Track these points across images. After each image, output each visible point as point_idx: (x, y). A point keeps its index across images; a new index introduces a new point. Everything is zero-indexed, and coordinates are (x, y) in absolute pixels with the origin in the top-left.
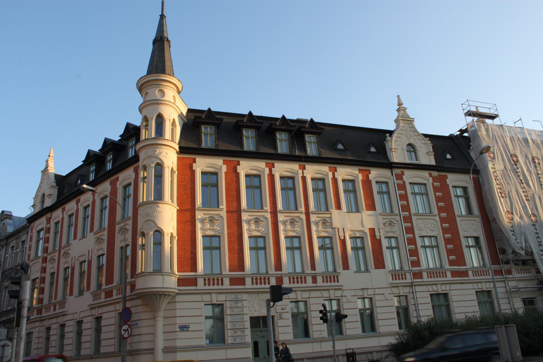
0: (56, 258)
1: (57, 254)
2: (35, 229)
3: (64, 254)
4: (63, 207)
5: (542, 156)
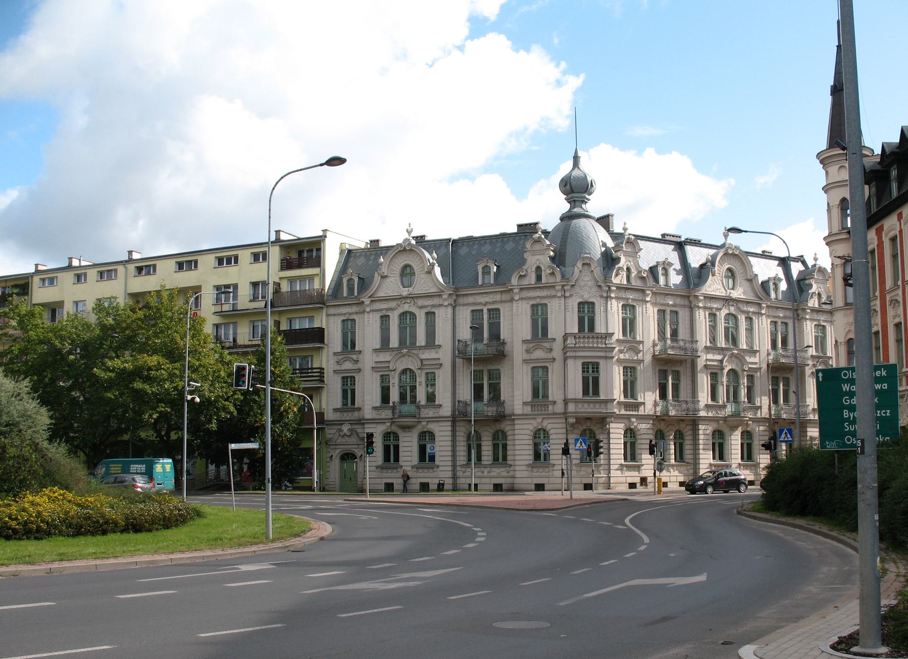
0: (900, 299)
1: (900, 292)
2: (886, 236)
3: (891, 301)
4: (898, 211)
5: (888, 425)
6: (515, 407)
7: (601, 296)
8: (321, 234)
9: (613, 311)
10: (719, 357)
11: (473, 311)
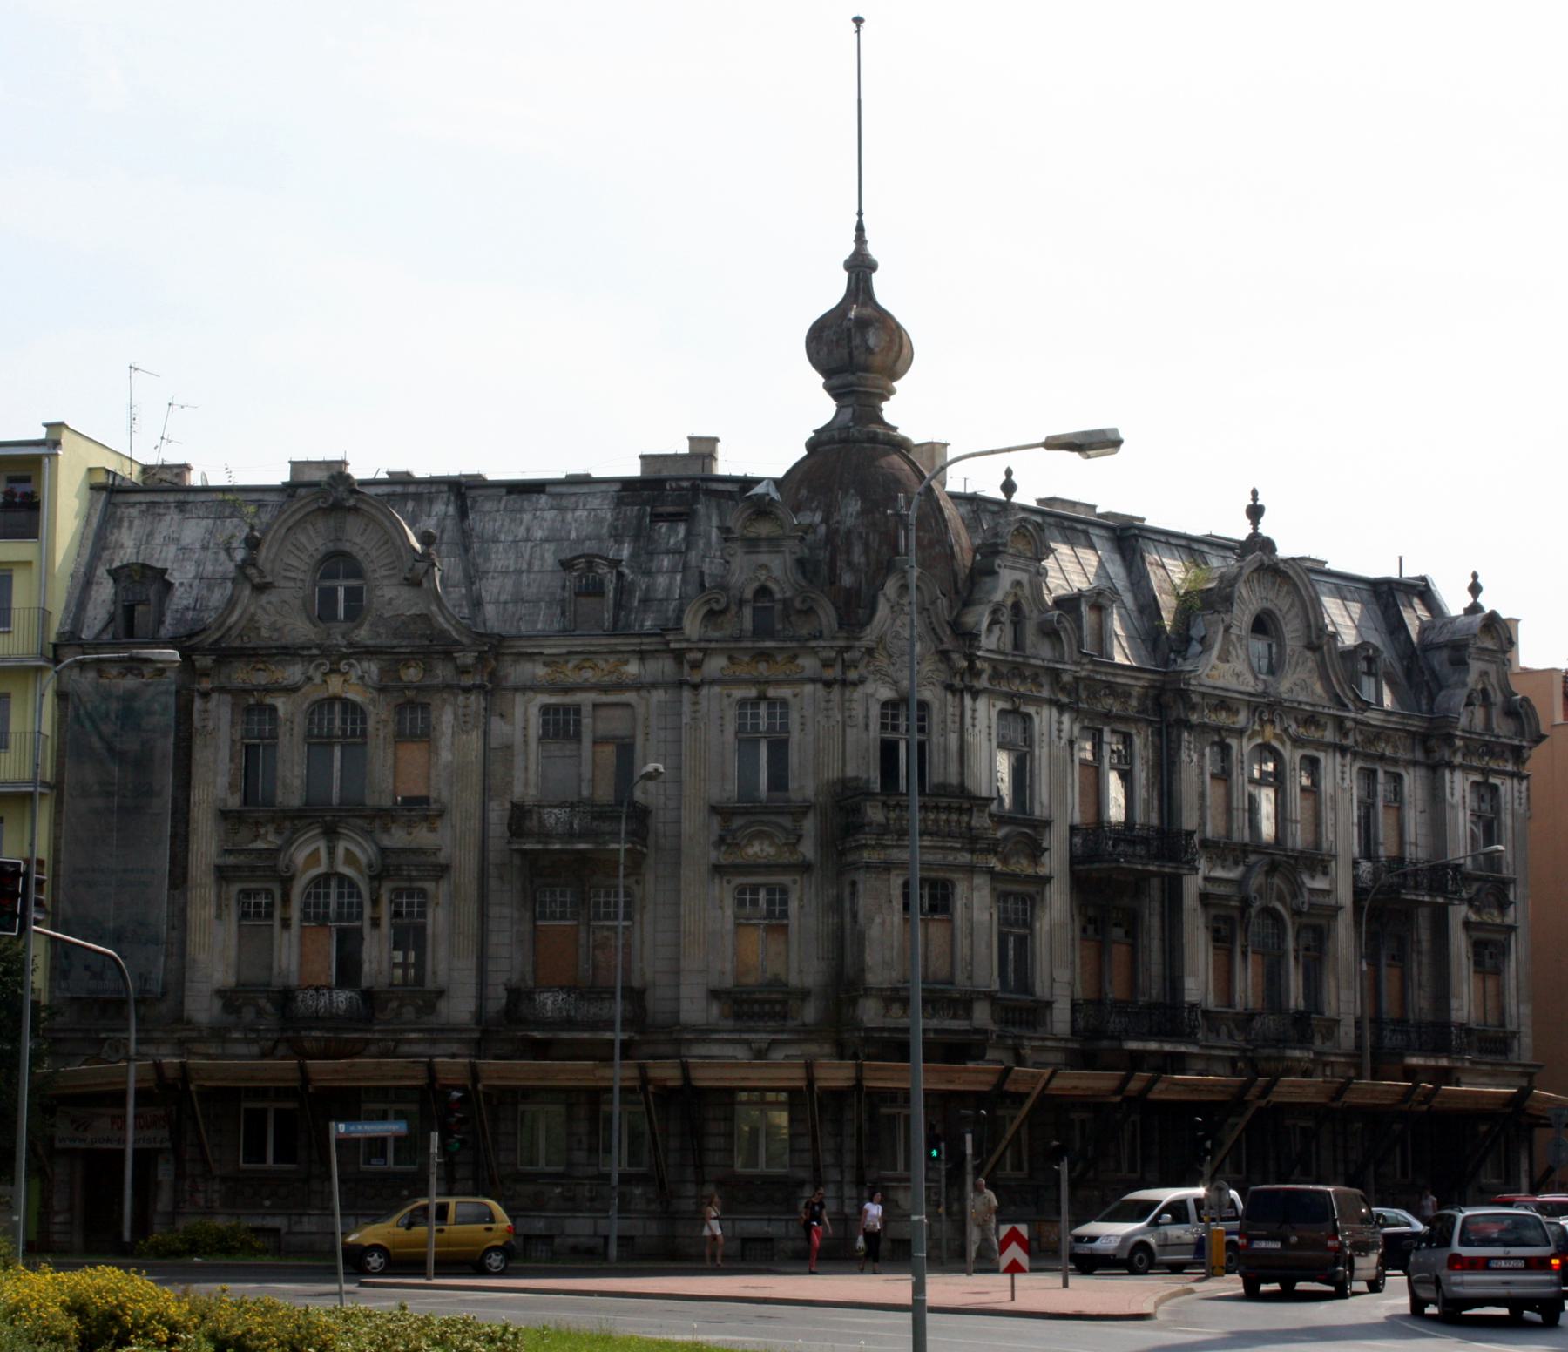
6: (685, 1005)
7: (949, 688)
8: (41, 434)
9: (977, 729)
10: (1234, 874)
11: (545, 709)
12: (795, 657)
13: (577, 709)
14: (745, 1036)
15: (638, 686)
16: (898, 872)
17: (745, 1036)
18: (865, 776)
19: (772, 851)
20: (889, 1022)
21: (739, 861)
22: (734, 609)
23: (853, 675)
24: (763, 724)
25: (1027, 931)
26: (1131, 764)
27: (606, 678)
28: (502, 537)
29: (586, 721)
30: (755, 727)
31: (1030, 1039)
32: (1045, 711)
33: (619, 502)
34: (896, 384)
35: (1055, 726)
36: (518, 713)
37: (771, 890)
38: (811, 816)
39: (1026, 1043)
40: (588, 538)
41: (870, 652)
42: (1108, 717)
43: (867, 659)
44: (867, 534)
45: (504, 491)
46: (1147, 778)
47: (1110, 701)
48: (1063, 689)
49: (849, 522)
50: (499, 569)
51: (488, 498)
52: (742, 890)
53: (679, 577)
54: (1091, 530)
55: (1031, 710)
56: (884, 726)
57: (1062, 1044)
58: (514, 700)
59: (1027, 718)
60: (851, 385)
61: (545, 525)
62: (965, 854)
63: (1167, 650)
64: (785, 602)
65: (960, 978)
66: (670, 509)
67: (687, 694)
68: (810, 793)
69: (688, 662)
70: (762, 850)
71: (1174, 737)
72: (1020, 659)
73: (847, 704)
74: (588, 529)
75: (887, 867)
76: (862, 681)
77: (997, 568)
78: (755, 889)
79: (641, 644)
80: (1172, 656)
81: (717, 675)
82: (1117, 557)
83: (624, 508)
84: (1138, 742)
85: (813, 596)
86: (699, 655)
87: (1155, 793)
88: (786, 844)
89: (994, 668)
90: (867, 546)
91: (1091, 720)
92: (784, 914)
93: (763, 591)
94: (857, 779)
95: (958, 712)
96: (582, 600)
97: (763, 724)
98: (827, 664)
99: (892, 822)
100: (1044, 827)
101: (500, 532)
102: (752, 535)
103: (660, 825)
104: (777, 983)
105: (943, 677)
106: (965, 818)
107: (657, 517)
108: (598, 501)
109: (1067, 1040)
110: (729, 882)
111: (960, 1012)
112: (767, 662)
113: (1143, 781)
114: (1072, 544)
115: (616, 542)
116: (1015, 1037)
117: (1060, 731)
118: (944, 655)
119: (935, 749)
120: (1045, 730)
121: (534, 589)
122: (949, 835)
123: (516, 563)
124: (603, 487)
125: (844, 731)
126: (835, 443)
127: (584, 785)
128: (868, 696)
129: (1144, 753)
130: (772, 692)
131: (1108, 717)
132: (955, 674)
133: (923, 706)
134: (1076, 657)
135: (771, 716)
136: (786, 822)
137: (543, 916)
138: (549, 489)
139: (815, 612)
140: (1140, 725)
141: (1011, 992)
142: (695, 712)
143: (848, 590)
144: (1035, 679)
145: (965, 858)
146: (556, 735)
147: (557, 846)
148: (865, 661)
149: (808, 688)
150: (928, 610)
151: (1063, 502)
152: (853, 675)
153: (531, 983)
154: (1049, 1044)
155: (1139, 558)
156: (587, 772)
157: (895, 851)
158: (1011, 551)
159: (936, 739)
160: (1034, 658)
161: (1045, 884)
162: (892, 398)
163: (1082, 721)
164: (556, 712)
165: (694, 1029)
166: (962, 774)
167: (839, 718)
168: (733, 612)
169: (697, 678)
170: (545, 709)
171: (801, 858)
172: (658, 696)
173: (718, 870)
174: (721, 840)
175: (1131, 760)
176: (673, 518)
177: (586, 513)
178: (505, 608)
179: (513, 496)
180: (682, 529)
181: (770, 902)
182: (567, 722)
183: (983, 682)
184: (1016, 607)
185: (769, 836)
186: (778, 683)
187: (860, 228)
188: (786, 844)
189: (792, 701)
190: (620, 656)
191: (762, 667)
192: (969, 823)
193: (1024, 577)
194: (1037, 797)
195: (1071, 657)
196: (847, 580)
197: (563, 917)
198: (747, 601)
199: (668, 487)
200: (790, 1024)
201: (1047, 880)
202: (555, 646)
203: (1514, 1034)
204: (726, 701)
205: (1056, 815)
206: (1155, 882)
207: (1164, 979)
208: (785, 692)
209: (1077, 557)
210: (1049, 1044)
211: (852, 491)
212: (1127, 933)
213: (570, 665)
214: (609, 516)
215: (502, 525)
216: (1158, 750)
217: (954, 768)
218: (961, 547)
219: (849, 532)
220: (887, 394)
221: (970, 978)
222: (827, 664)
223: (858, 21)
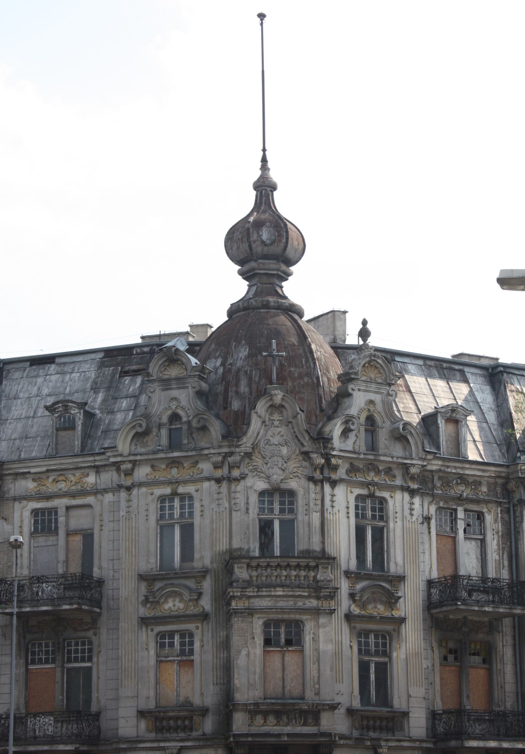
6: (122, 723)
7: (311, 479)
9: (335, 510)
11: (35, 512)
12: (197, 462)
13: (54, 511)
14: (162, 744)
15: (96, 492)
16: (257, 616)
17: (162, 744)
18: (246, 547)
19: (181, 606)
20: (254, 730)
21: (158, 614)
22: (155, 431)
23: (236, 473)
24: (177, 513)
25: (386, 659)
26: (484, 535)
27: (73, 488)
28: (21, 395)
29: (62, 519)
30: (171, 516)
31: (387, 740)
32: (398, 495)
33: (102, 365)
34: (292, 268)
35: (407, 506)
36: (17, 515)
37: (182, 635)
38: (208, 578)
39: (383, 743)
40: (77, 392)
41: (248, 455)
42: (460, 500)
43: (247, 460)
44: (251, 371)
45: (28, 364)
46: (498, 544)
47: (462, 488)
48: (413, 478)
49: (239, 364)
50: (15, 417)
51: (17, 369)
52: (162, 635)
53: (131, 414)
54: (466, 369)
55: (386, 495)
56: (262, 510)
57: (417, 744)
58: (13, 507)
59: (383, 501)
60: (253, 269)
61: (51, 384)
62: (312, 600)
63: (516, 450)
64: (189, 423)
65: (310, 695)
66: (134, 367)
67: (123, 494)
68: (207, 562)
69: (123, 471)
70: (174, 605)
71: (518, 514)
72: (372, 457)
73: (233, 495)
74: (78, 385)
75: (251, 612)
76: (243, 477)
77: (350, 391)
78: (171, 635)
79: (95, 461)
80: (519, 454)
81: (144, 480)
82: (487, 389)
83: (104, 369)
84: (489, 518)
85: (205, 417)
86: (129, 466)
87: (505, 556)
88: (190, 600)
89: (351, 464)
90: (250, 379)
91: (446, 502)
92: (191, 652)
93: (175, 417)
94: (240, 549)
95: (319, 497)
96: (62, 433)
97: (177, 513)
98: (216, 466)
99: (254, 579)
100: (399, 581)
101: (21, 392)
102: (166, 377)
103: (110, 592)
104: (187, 705)
105: (308, 472)
106: (312, 574)
107: (125, 373)
108: (87, 366)
109: (421, 741)
110: (152, 630)
111: (310, 721)
112: (178, 468)
113: (495, 547)
114: (448, 379)
115: (94, 393)
116: (372, 739)
117: (412, 509)
118: (306, 455)
119: (301, 526)
120: (399, 509)
121: (35, 429)
122: (299, 587)
123: (27, 412)
124: (93, 356)
125: (231, 514)
126: (241, 311)
127: (60, 565)
128: (247, 488)
129: (495, 526)
130: (181, 490)
131: (460, 500)
132: (315, 470)
133: (292, 493)
134: (422, 454)
135: (182, 507)
136: (191, 583)
137: (33, 662)
138: (57, 360)
139: (208, 429)
140: (490, 505)
141: (373, 706)
142: (128, 507)
143: (236, 413)
144: (388, 471)
145: (313, 603)
146: (43, 530)
147: (28, 609)
148: (246, 462)
149: (206, 485)
150: (291, 422)
151: (469, 355)
152: (236, 473)
153: (23, 711)
154: (406, 744)
155: (503, 388)
156: (62, 557)
157: (257, 600)
158: (363, 378)
159: (301, 517)
160: (385, 455)
161: (401, 623)
162: (290, 278)
163: (438, 503)
164: (43, 514)
165: (127, 740)
166: (323, 543)
167: (227, 505)
168: (155, 434)
169: (129, 483)
170: (35, 512)
171: (201, 610)
172: (109, 497)
173: (144, 622)
174: (146, 600)
175: (484, 532)
176: (136, 373)
177: (78, 374)
178: (14, 443)
179: (34, 367)
180: (139, 380)
181: (182, 644)
182: (50, 521)
183: (342, 473)
184: (370, 420)
185: (180, 595)
186: (185, 482)
187: (264, 160)
188: (190, 600)
189: (194, 494)
190: (83, 471)
191: (174, 471)
192: (315, 577)
193: (377, 398)
194: (392, 559)
195: (418, 454)
196: (236, 405)
197: (47, 662)
198: (165, 425)
199: (135, 352)
200: (194, 734)
201: (402, 620)
202: (38, 466)
203: (405, 714)
204: (150, 498)
205: (409, 573)
206: (507, 622)
207: (517, 695)
208: (190, 489)
209: (450, 388)
210: (406, 744)
211: (243, 342)
212: (484, 661)
213: (51, 480)
214: (93, 374)
215: (23, 387)
216: (506, 524)
217: (316, 539)
218: (329, 379)
219: (239, 370)
220: (285, 276)
221: (318, 694)
222: (216, 466)
223: (262, 16)
